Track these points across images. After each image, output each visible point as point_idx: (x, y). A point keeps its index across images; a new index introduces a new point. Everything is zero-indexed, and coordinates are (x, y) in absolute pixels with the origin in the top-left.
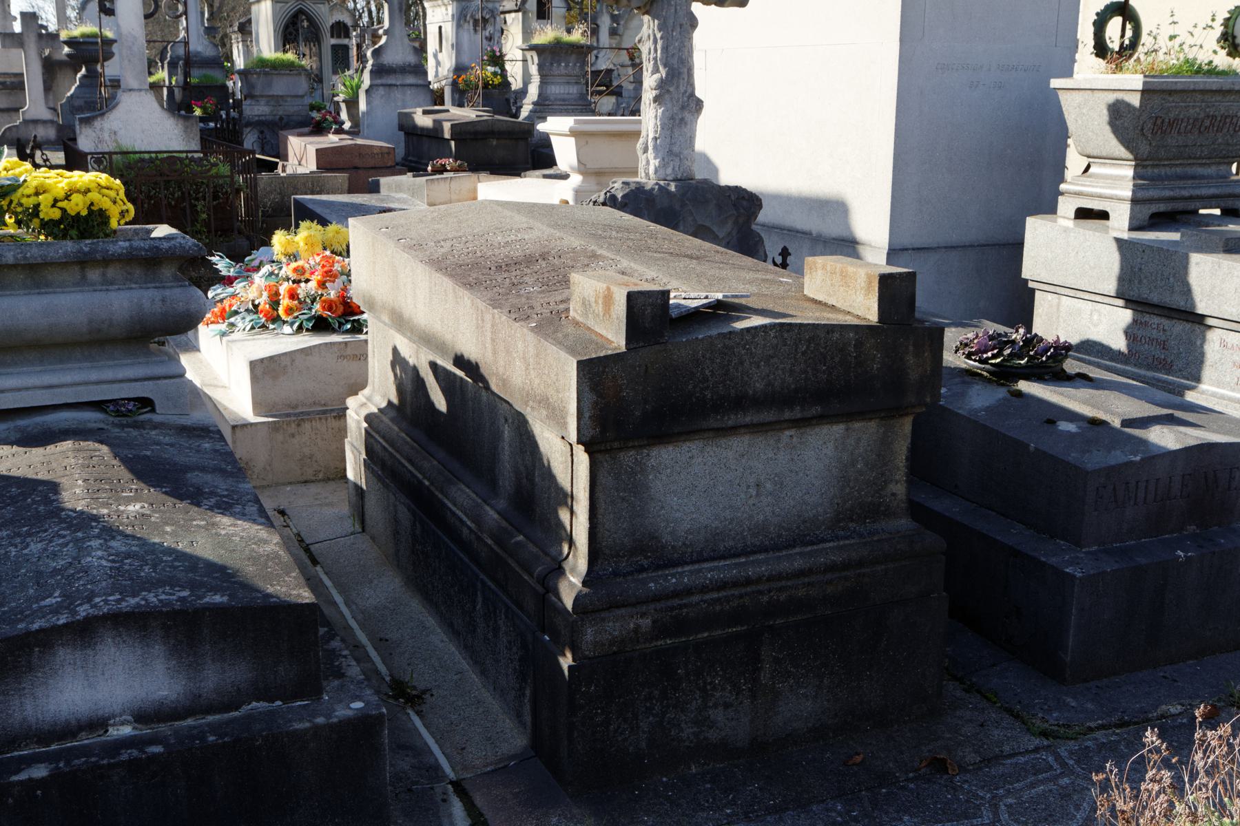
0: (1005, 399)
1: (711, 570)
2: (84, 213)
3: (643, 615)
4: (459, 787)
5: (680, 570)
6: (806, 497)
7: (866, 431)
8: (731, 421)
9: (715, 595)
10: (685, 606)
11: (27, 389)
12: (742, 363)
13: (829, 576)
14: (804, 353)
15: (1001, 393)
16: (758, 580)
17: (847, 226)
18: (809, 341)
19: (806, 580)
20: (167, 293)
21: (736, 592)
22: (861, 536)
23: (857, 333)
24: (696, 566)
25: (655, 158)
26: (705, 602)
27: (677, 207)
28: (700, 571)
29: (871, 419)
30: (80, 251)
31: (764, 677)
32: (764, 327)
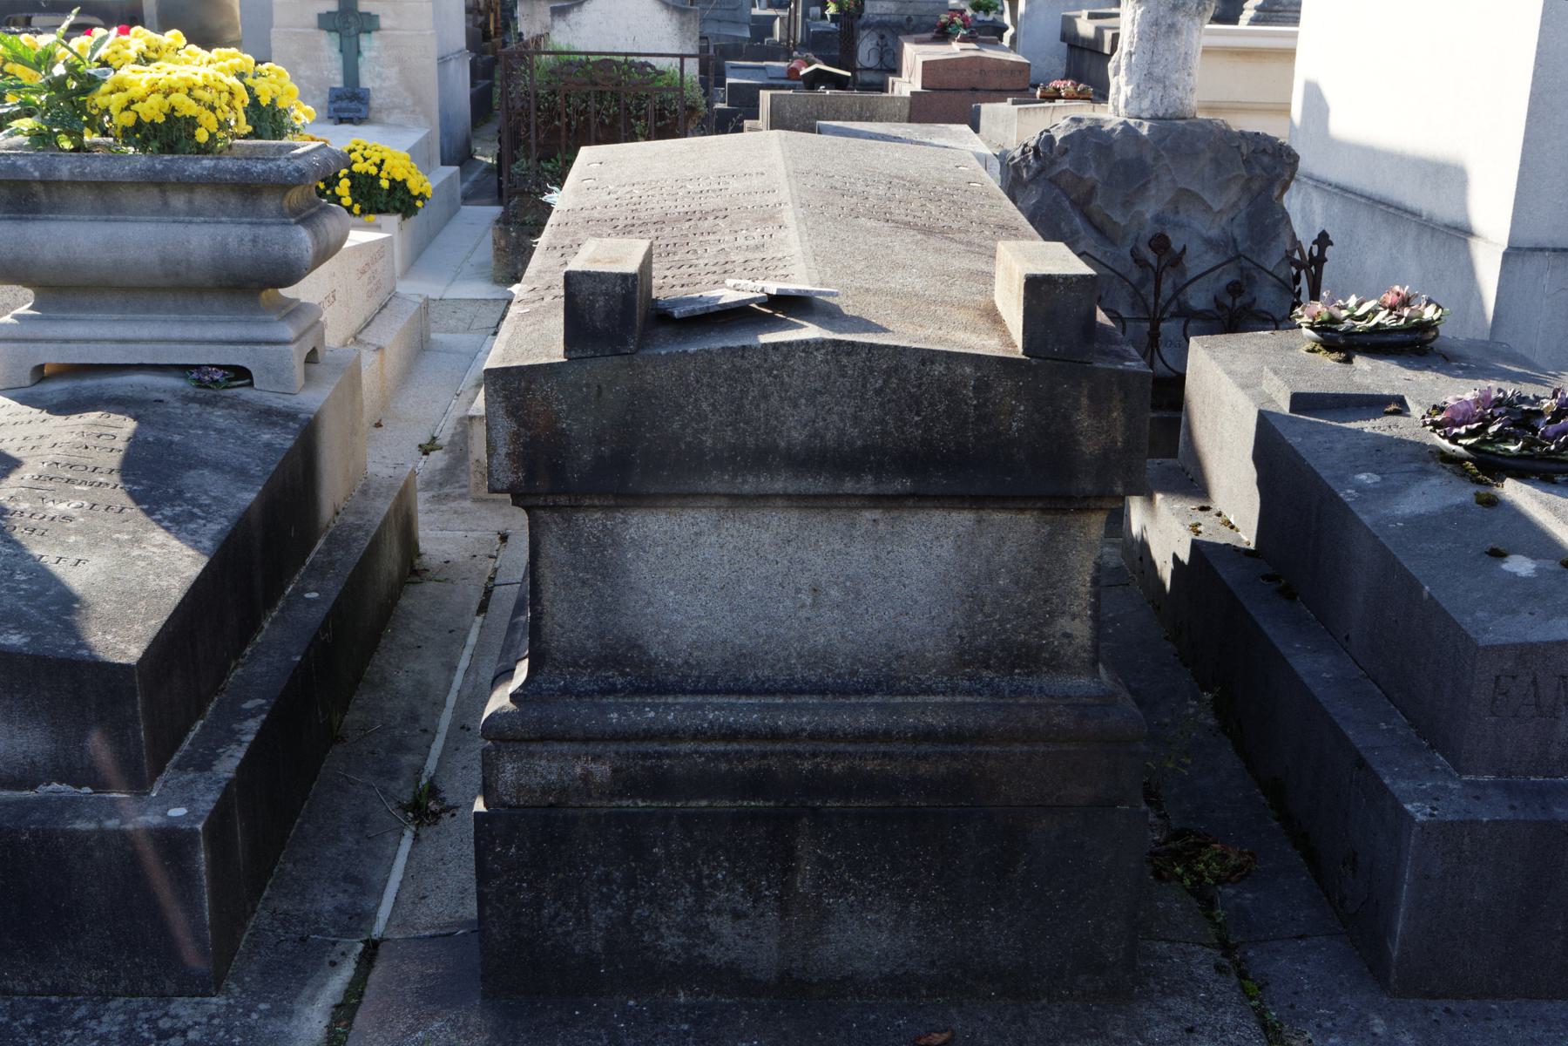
0: (1462, 508)
1: (720, 708)
2: (161, 119)
3: (596, 758)
4: (372, 949)
5: (670, 700)
6: (903, 619)
7: (1014, 531)
8: (749, 485)
9: (721, 747)
10: (668, 755)
11: (97, 341)
12: (765, 397)
13: (925, 748)
14: (878, 392)
15: (1465, 494)
16: (795, 735)
17: (1463, 206)
18: (888, 374)
19: (882, 748)
20: (262, 231)
21: (755, 747)
22: (997, 693)
23: (977, 368)
24: (699, 699)
25: (1127, 84)
26: (701, 754)
27: (1149, 160)
28: (701, 706)
29: (1022, 510)
30: (151, 169)
31: (803, 881)
32: (820, 344)
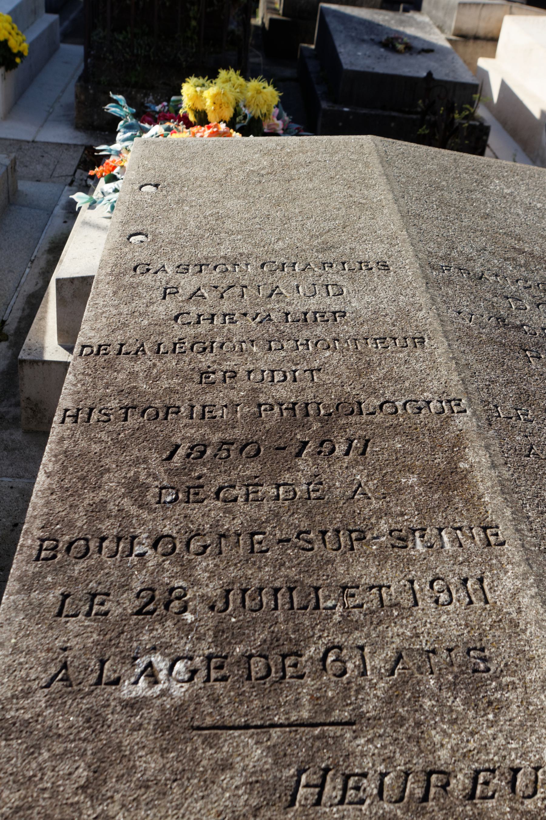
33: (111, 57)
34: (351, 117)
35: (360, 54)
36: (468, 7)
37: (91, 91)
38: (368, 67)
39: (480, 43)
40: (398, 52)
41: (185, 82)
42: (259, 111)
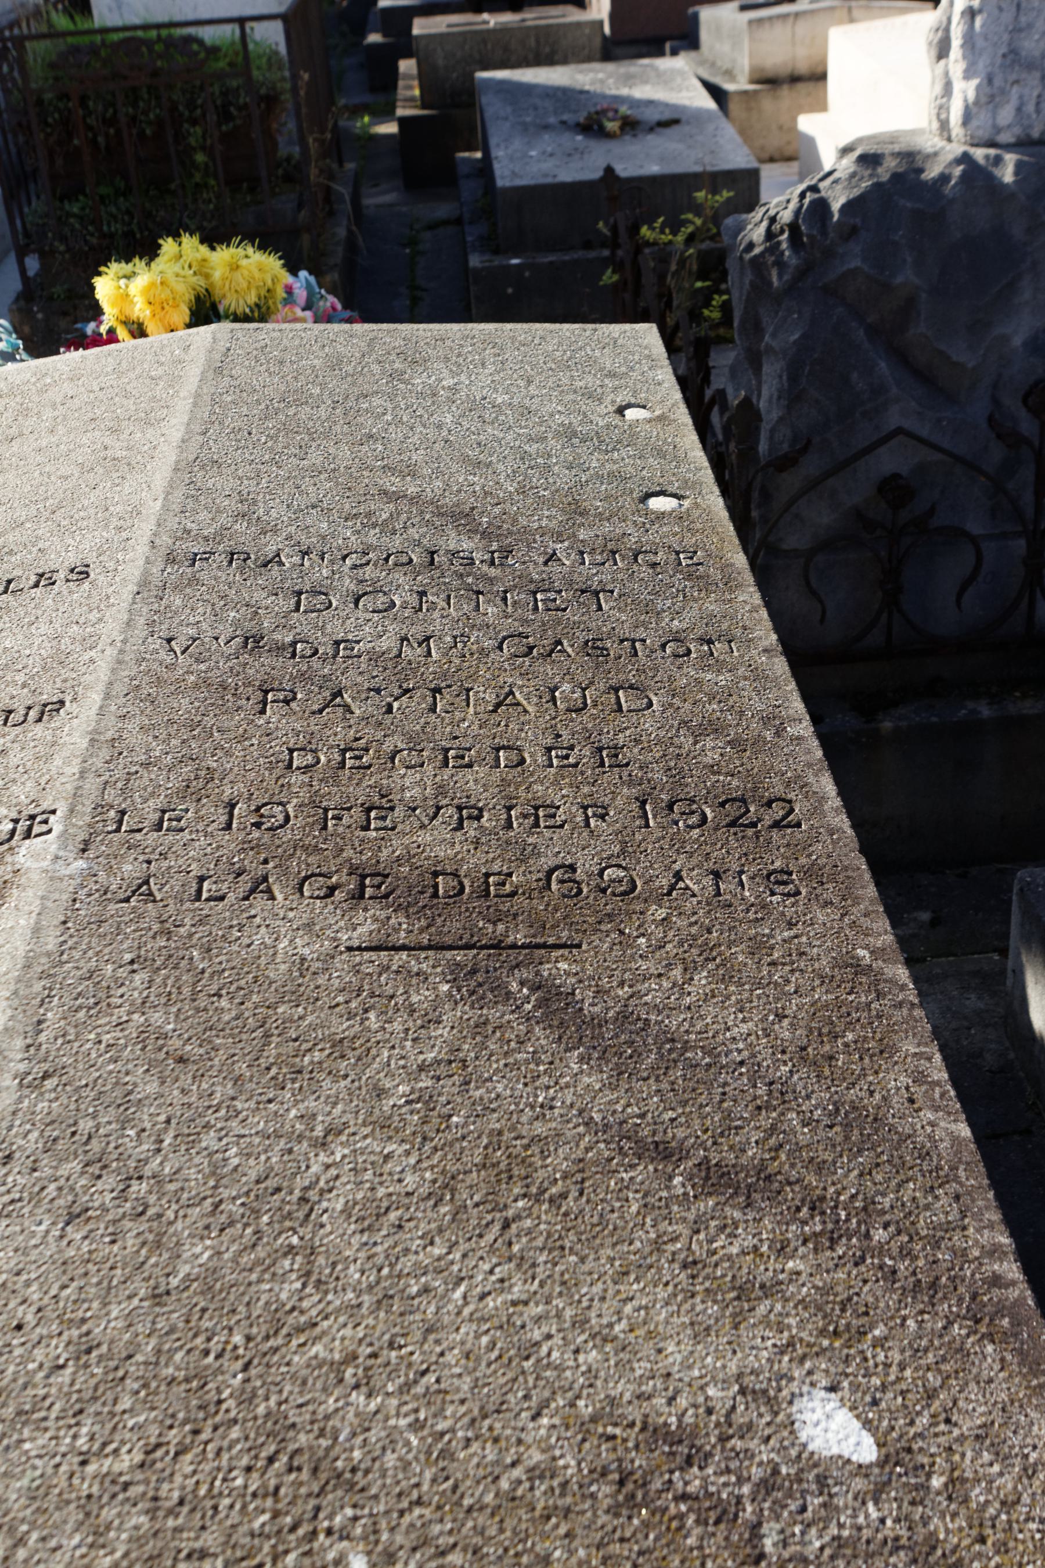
25: (967, 75)
33: (62, 248)
34: (527, 274)
35: (533, 153)
36: (767, 25)
37: (40, 316)
38: (546, 175)
39: (800, 86)
40: (609, 136)
41: (99, 274)
42: (241, 302)
